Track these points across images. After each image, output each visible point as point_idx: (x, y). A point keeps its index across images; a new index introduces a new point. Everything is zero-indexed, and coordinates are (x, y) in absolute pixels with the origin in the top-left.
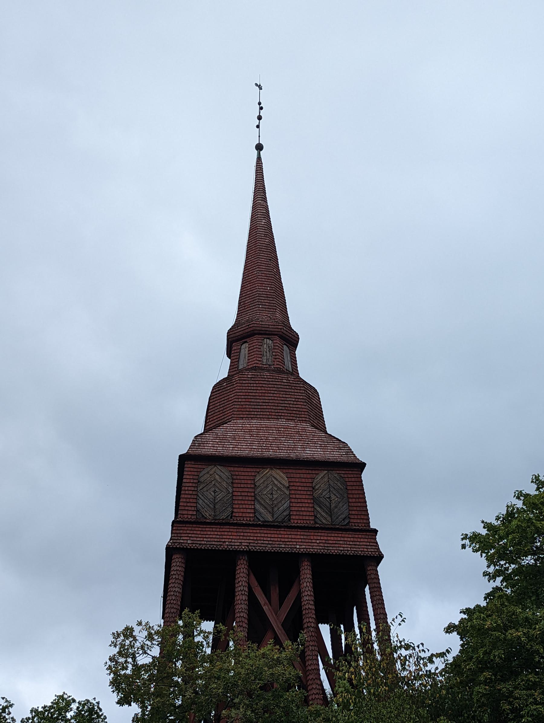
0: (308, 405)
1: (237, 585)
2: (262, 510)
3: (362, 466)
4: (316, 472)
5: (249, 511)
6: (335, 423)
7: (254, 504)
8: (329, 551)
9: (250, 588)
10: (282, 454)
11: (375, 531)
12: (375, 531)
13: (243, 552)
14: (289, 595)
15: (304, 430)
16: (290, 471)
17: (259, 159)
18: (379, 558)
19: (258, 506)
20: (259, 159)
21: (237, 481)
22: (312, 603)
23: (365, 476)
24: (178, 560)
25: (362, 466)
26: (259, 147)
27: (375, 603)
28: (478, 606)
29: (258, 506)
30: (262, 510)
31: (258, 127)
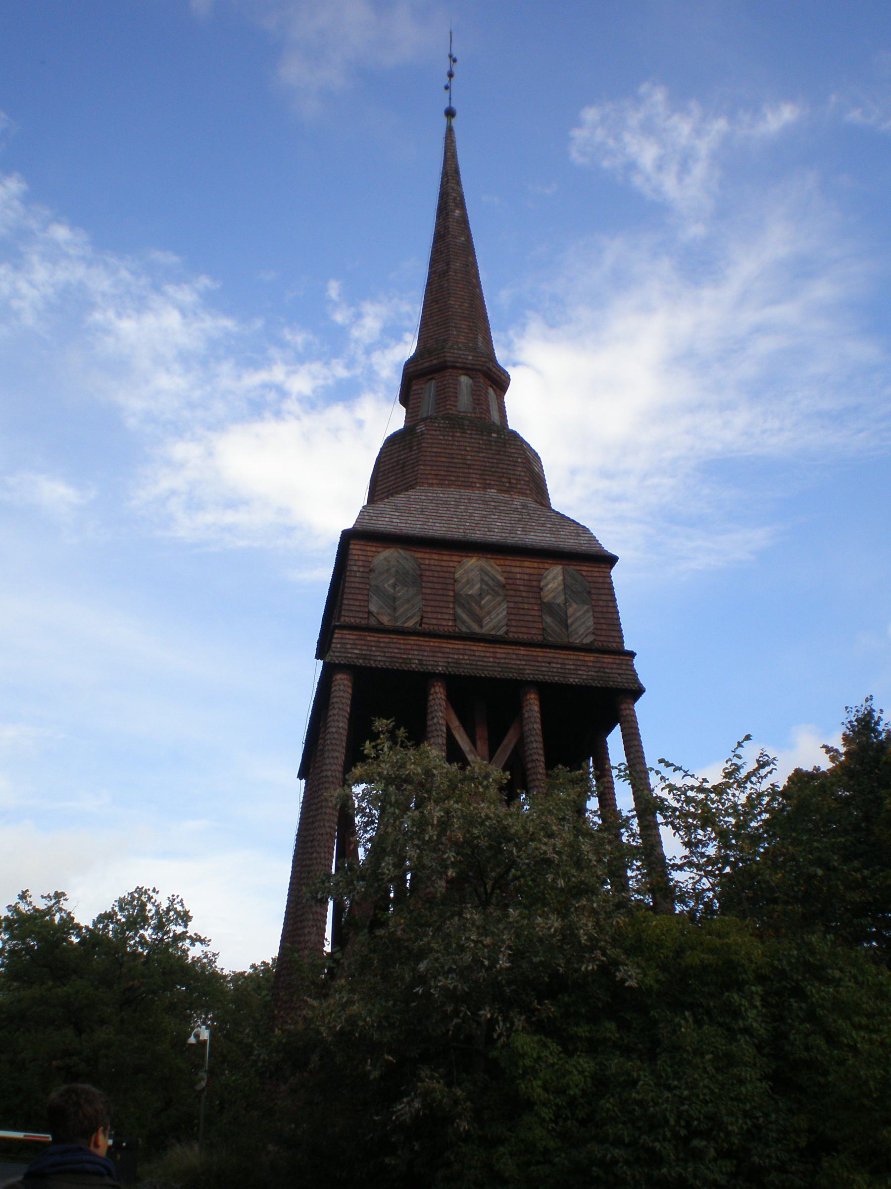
0: (516, 468)
1: (429, 723)
2: (465, 617)
3: (612, 560)
4: (546, 566)
5: (447, 617)
6: (563, 498)
7: (454, 608)
8: (377, 663)
9: (449, 729)
10: (477, 535)
11: (632, 654)
12: (632, 654)
13: (440, 674)
14: (505, 742)
15: (524, 506)
16: (507, 563)
17: (450, 130)
18: (637, 692)
19: (459, 611)
20: (450, 130)
21: (427, 573)
22: (541, 752)
23: (616, 574)
24: (343, 685)
25: (612, 560)
26: (450, 113)
27: (632, 756)
28: (817, 769)
29: (459, 611)
30: (465, 617)
31: (447, 88)
